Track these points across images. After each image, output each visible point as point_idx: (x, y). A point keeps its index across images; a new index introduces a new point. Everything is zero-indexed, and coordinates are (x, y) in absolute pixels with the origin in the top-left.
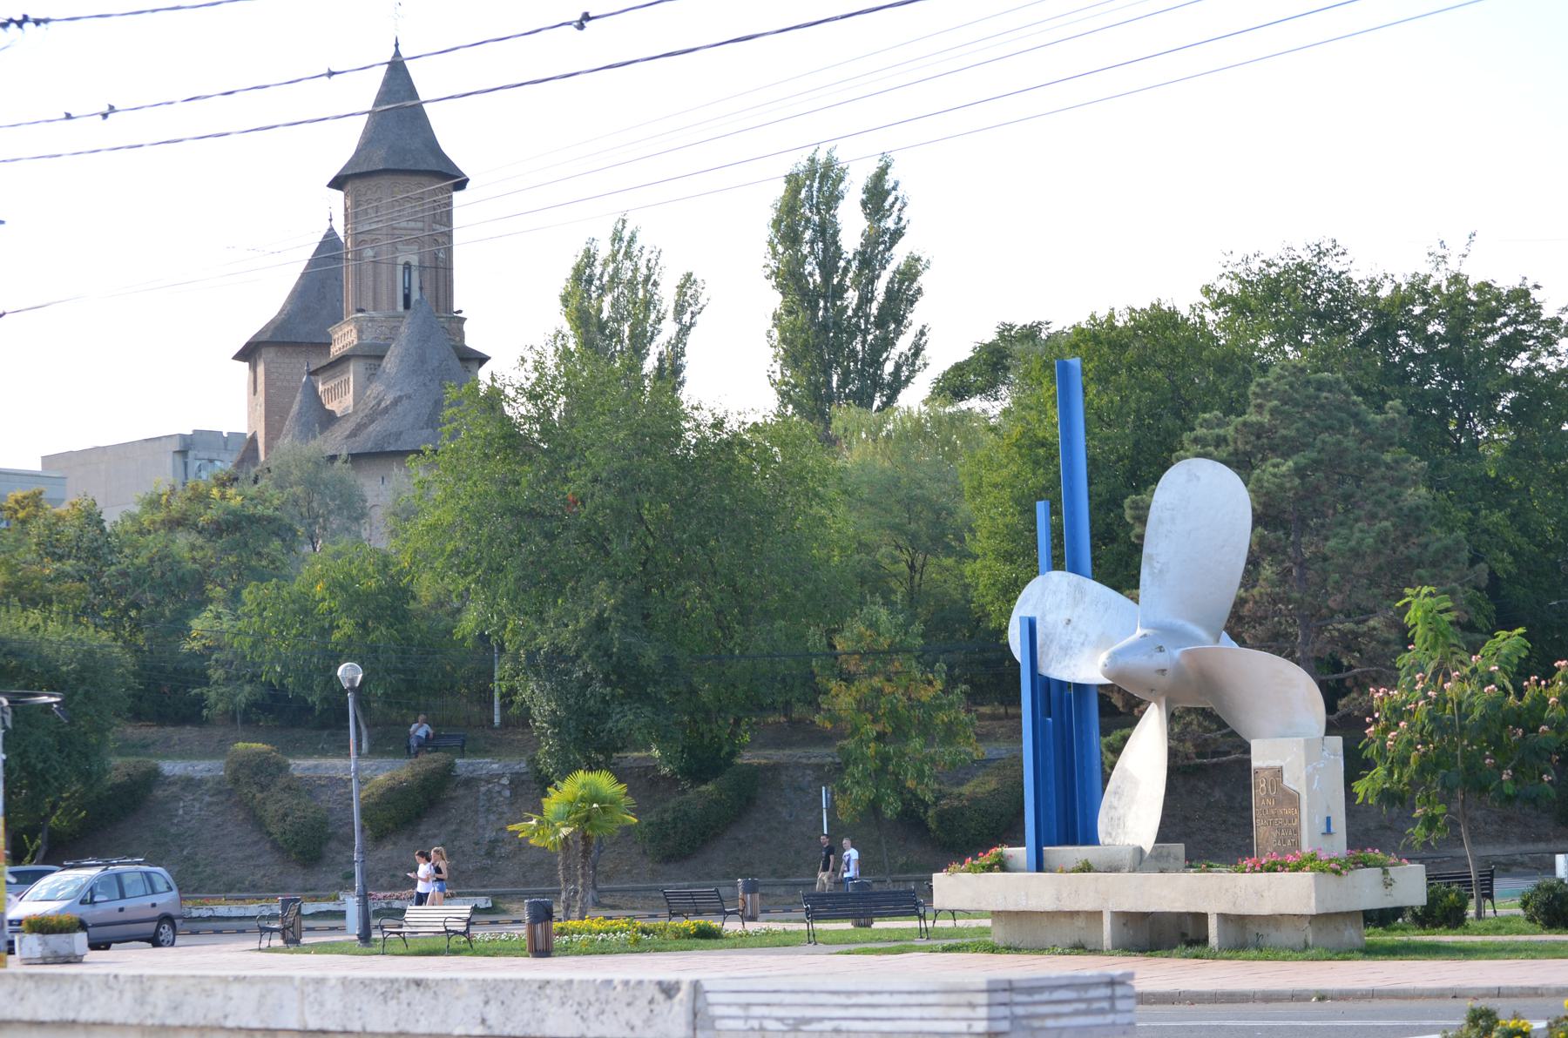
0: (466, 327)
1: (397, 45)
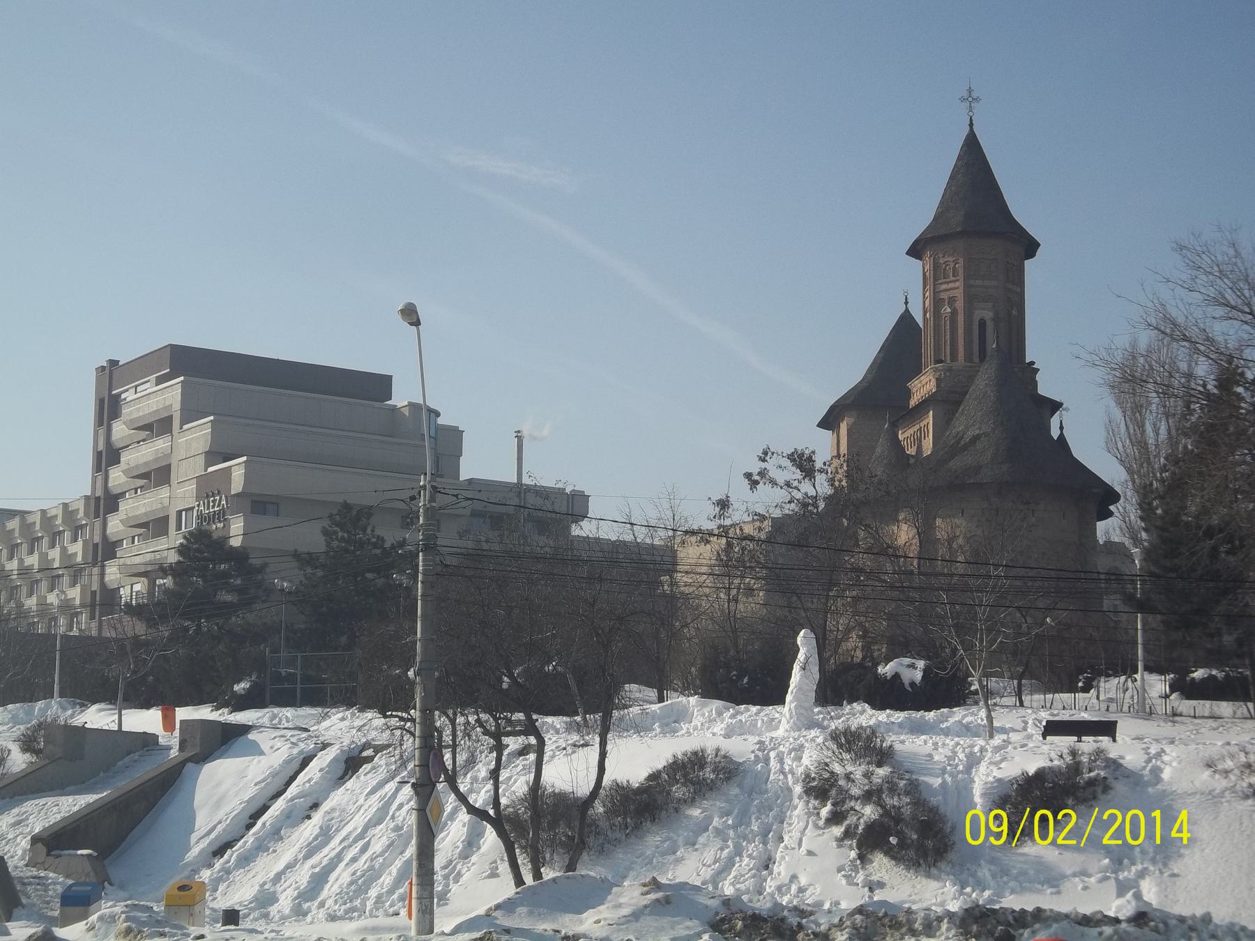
0: (1038, 377)
1: (971, 125)
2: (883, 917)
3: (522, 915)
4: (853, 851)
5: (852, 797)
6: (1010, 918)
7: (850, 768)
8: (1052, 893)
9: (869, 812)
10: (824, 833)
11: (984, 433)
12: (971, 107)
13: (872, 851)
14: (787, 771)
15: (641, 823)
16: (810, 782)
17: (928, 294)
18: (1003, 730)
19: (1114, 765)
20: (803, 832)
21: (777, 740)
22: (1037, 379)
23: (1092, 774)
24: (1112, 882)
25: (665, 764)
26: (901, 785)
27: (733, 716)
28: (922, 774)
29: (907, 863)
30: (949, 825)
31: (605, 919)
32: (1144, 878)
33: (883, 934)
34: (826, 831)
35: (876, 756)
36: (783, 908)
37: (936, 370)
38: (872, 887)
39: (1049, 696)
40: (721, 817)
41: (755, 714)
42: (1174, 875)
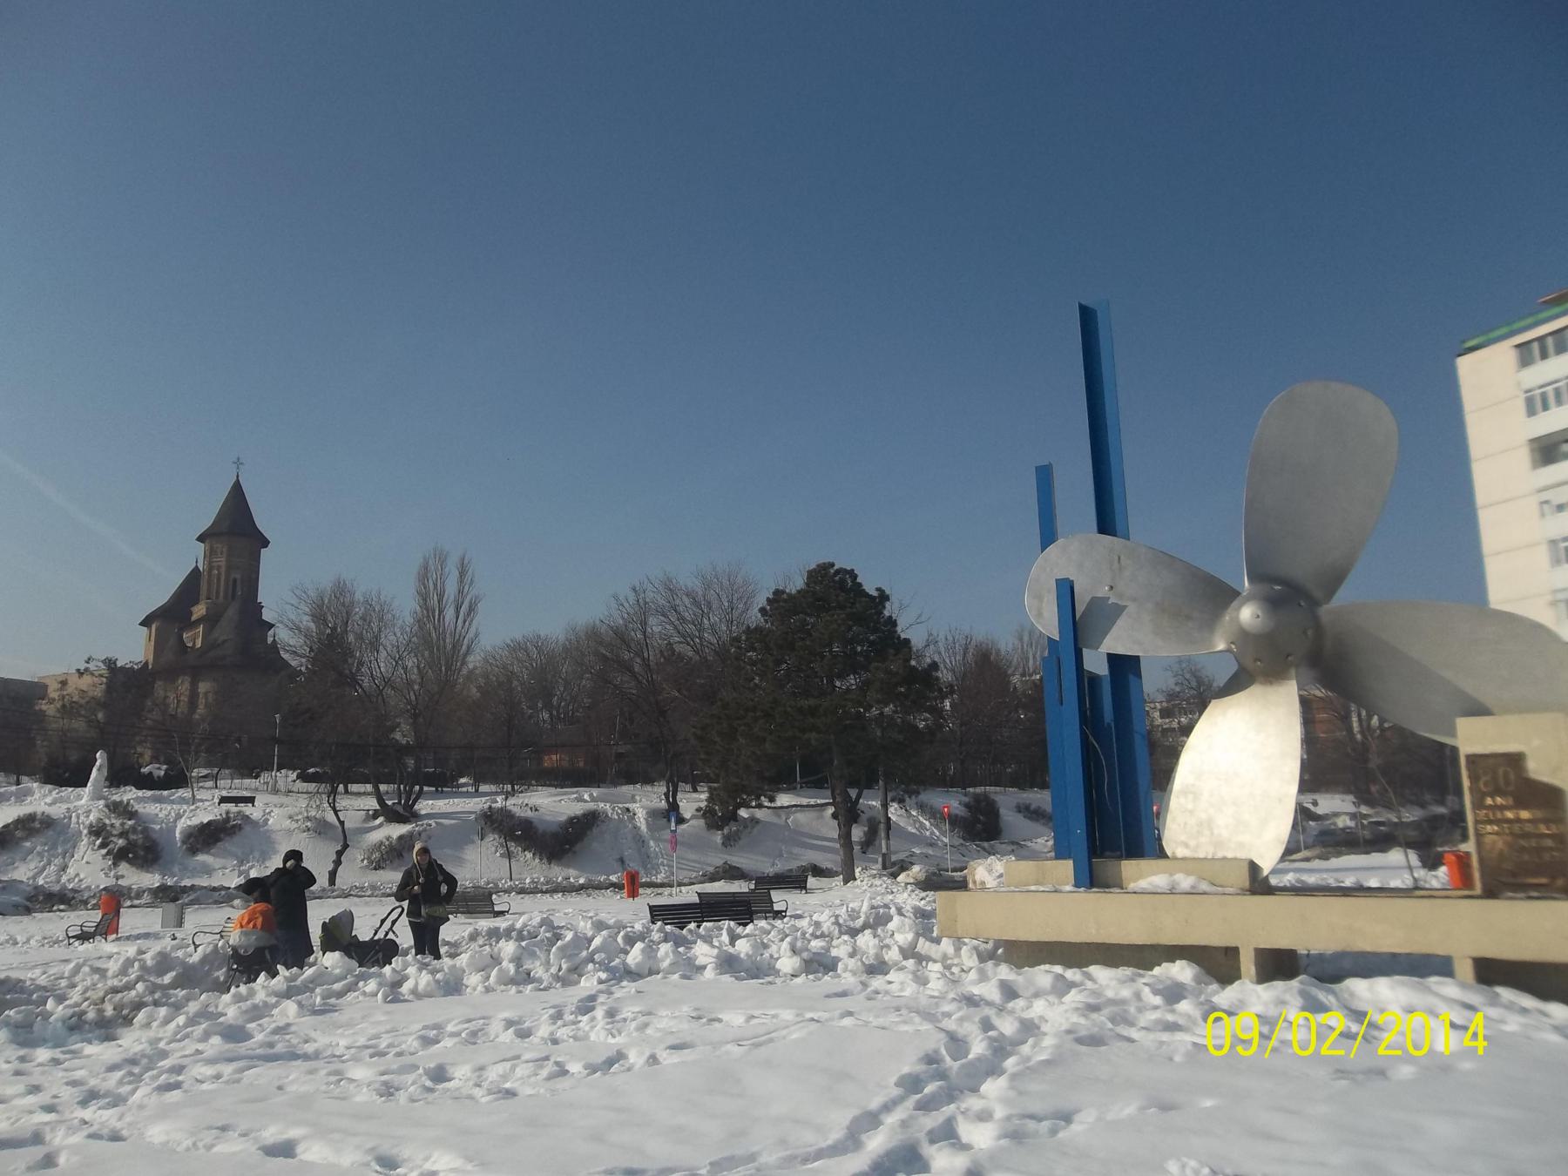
1: (238, 476)
5: (113, 835)
9: (121, 842)
20: (85, 853)
37: (207, 603)
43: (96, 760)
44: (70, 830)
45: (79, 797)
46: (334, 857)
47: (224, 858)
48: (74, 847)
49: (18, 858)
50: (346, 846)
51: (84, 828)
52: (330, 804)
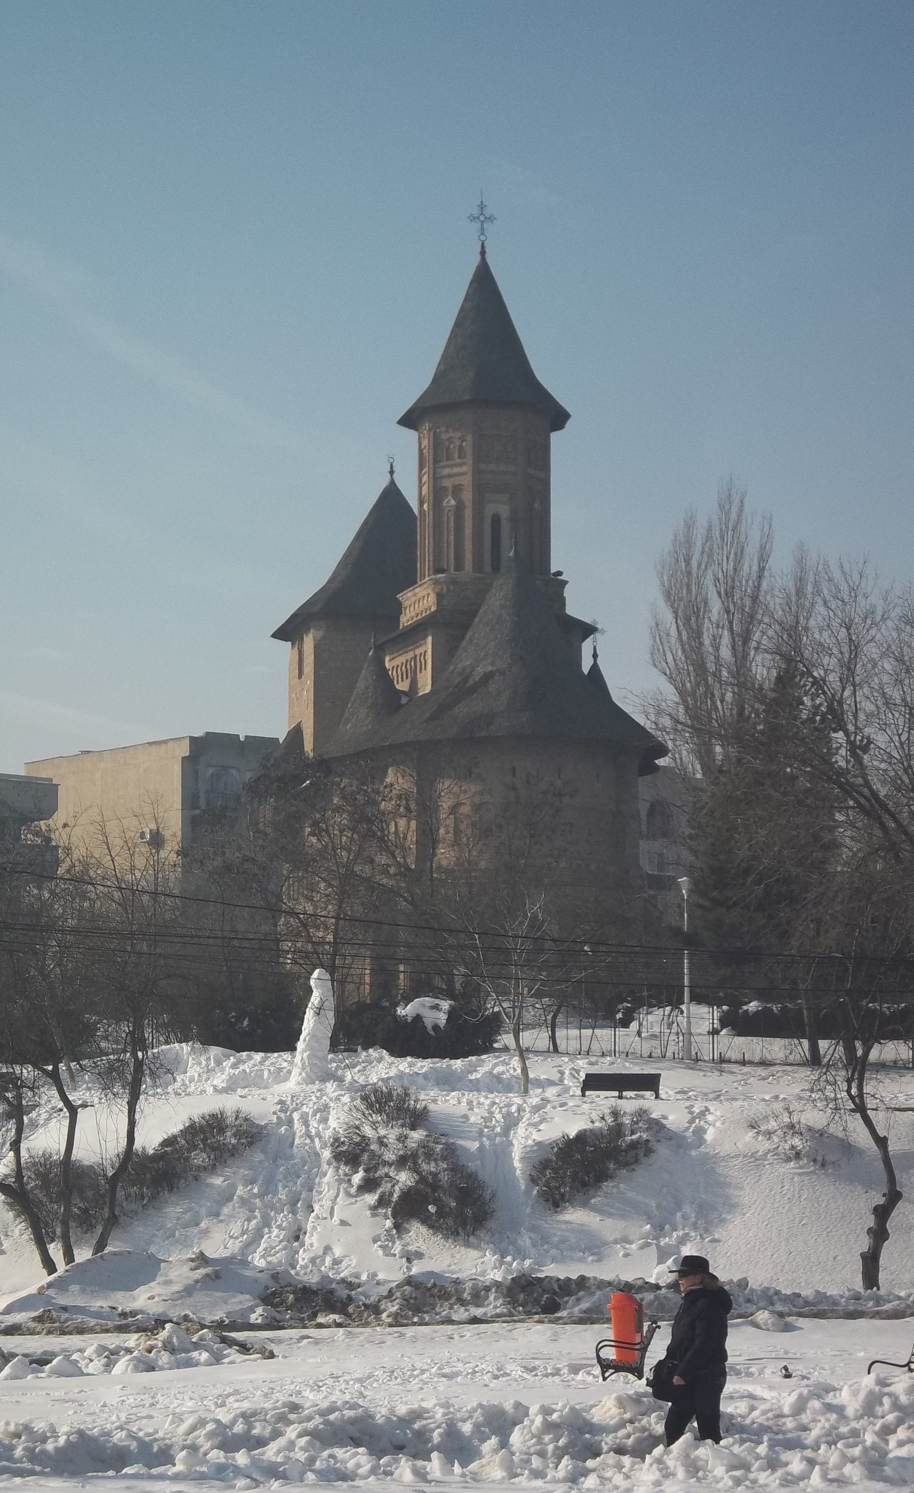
0: (567, 592)
1: (483, 253)
2: (432, 1288)
3: (76, 1293)
4: (388, 1221)
5: (386, 1163)
6: (556, 1287)
7: (382, 1132)
8: (593, 1261)
9: (405, 1178)
10: (356, 1201)
11: (498, 670)
12: (482, 229)
13: (408, 1220)
14: (313, 1134)
15: (158, 1192)
16: (339, 1146)
17: (425, 479)
18: (540, 1084)
19: (657, 1126)
20: (334, 1201)
21: (298, 1099)
22: (665, 1353)
23: (634, 1137)
24: (653, 1249)
25: (182, 1127)
26: (438, 1149)
27: (234, 1066)
28: (460, 1138)
29: (445, 1232)
30: (489, 1192)
31: (159, 1295)
32: (685, 1245)
33: (431, 1304)
34: (358, 1199)
35: (410, 1118)
36: (332, 1281)
37: (436, 582)
38: (410, 1257)
39: (587, 1032)
40: (245, 1186)
41: (260, 1063)
42: (715, 1241)
43: (310, 991)
44: (295, 1150)
45: (281, 1076)
46: (870, 1221)
47: (623, 1217)
48: (311, 1190)
49: (203, 1211)
50: (894, 1197)
51: (324, 1146)
52: (852, 1097)
